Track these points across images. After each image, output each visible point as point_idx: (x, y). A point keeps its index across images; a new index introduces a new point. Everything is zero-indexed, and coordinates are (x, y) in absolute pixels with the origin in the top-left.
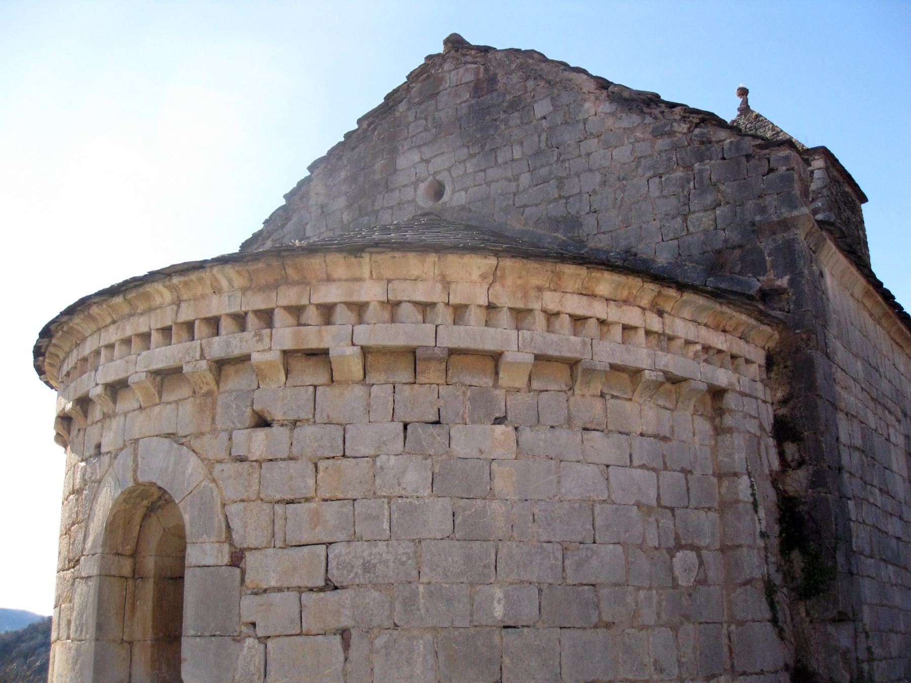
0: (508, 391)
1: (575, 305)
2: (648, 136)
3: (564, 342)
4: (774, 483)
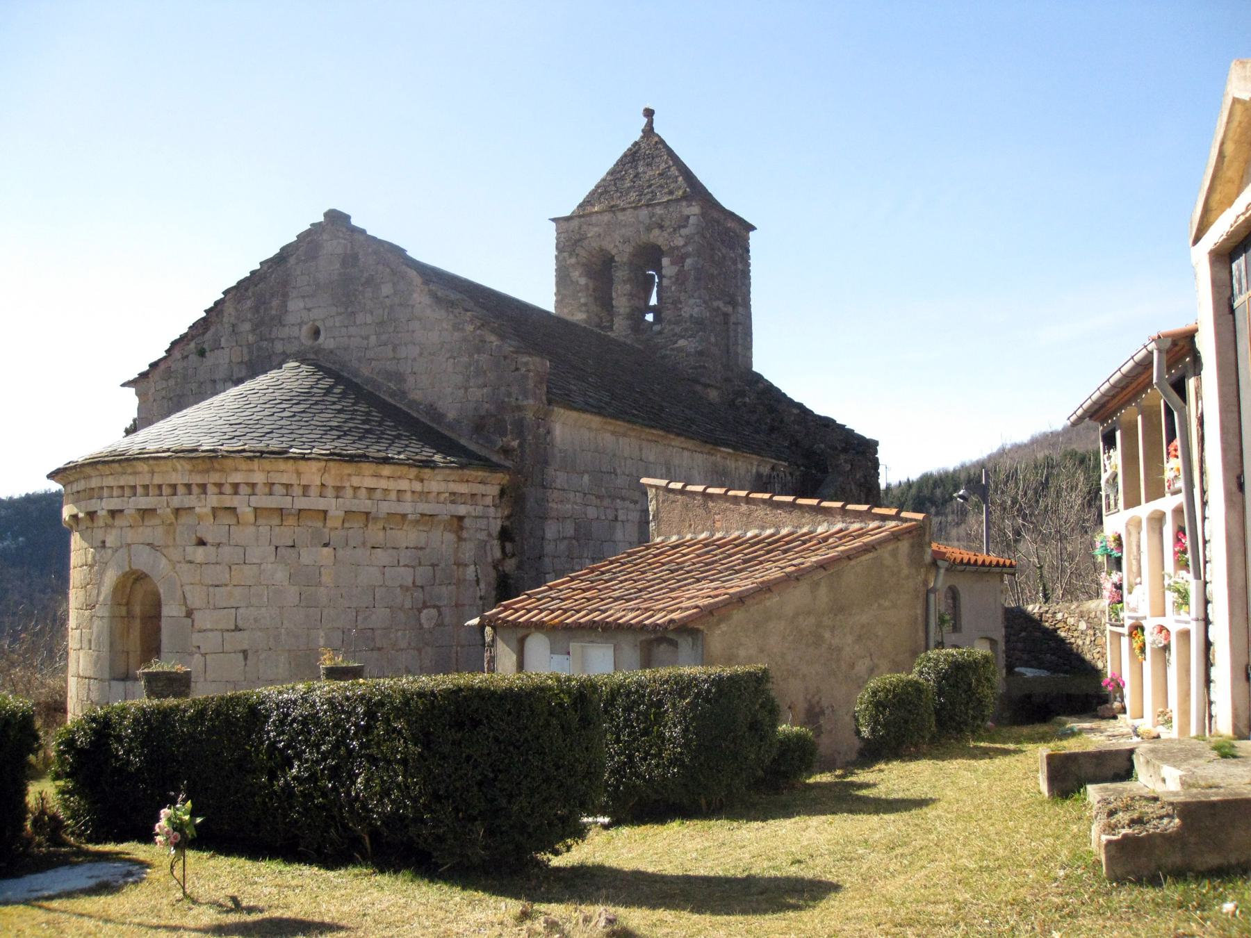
0: (331, 529)
1: (369, 482)
2: (450, 327)
3: (365, 504)
4: (495, 567)
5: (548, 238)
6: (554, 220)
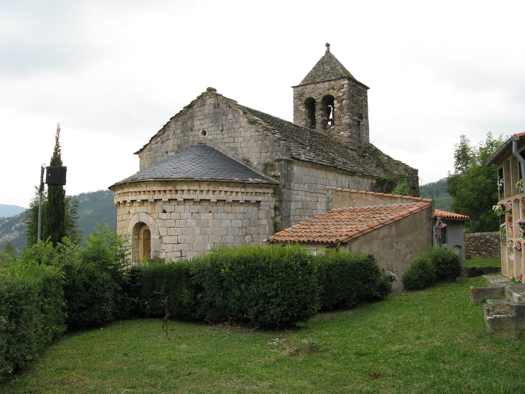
5: (291, 93)
6: (293, 87)
